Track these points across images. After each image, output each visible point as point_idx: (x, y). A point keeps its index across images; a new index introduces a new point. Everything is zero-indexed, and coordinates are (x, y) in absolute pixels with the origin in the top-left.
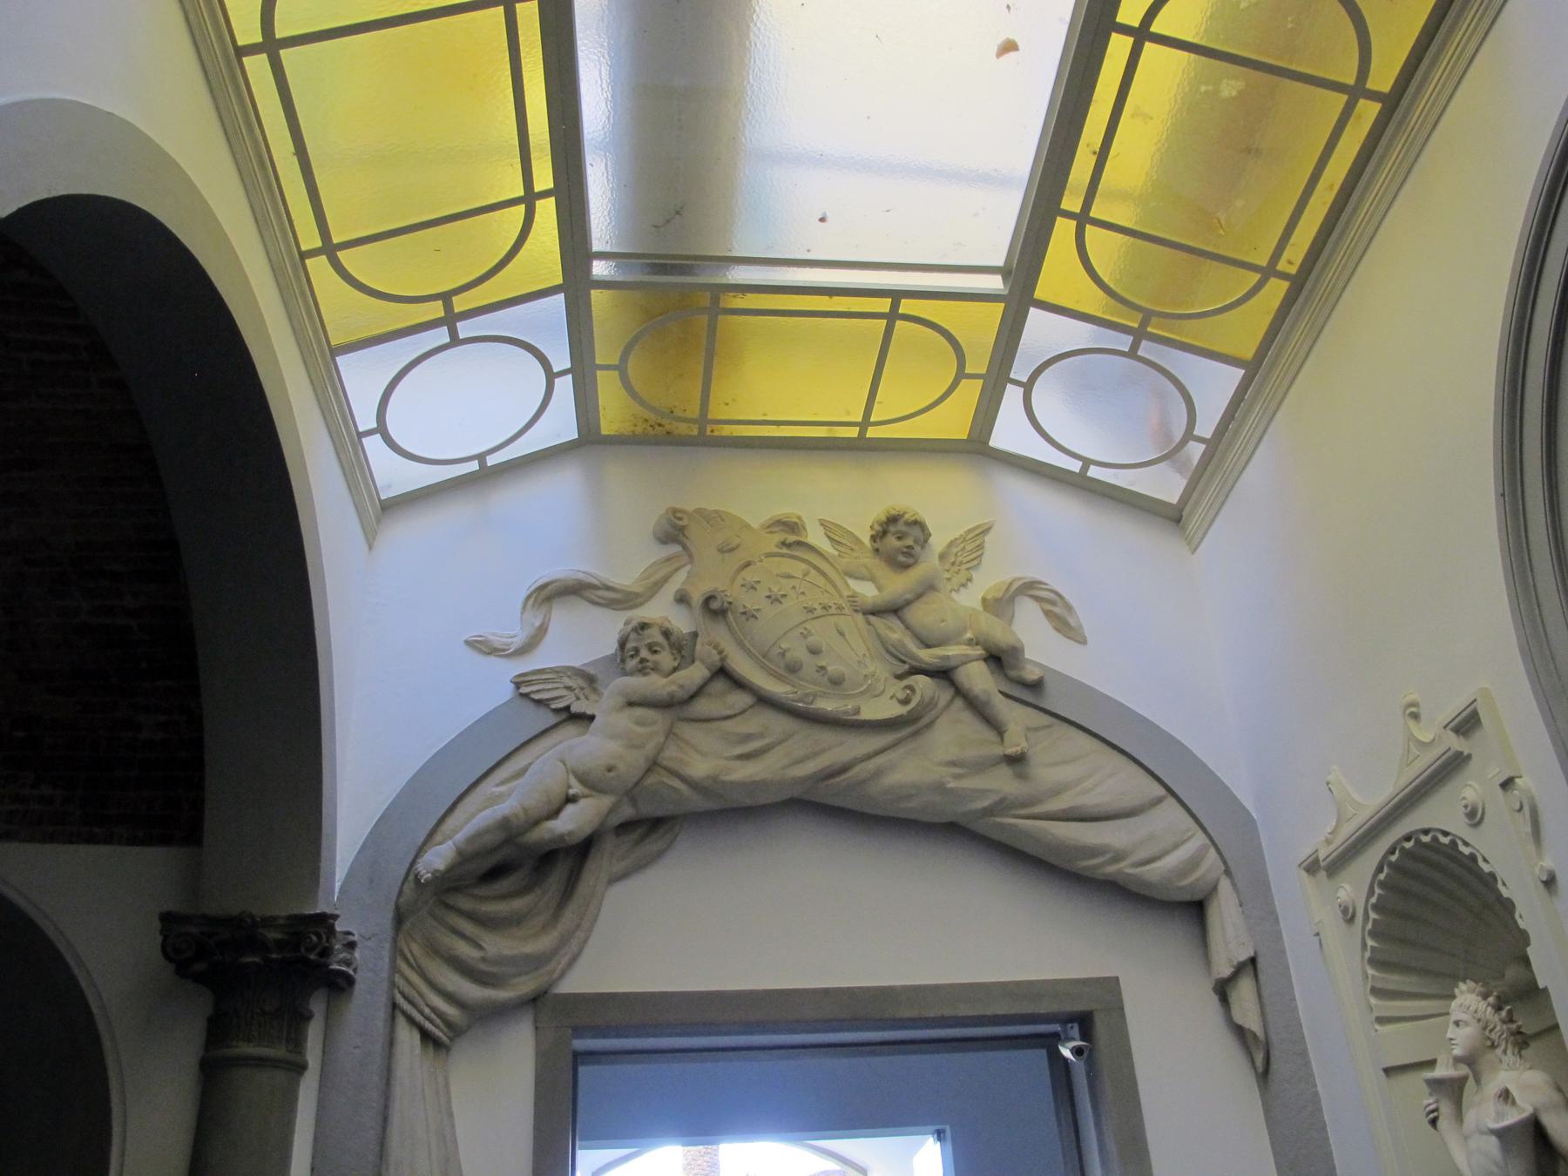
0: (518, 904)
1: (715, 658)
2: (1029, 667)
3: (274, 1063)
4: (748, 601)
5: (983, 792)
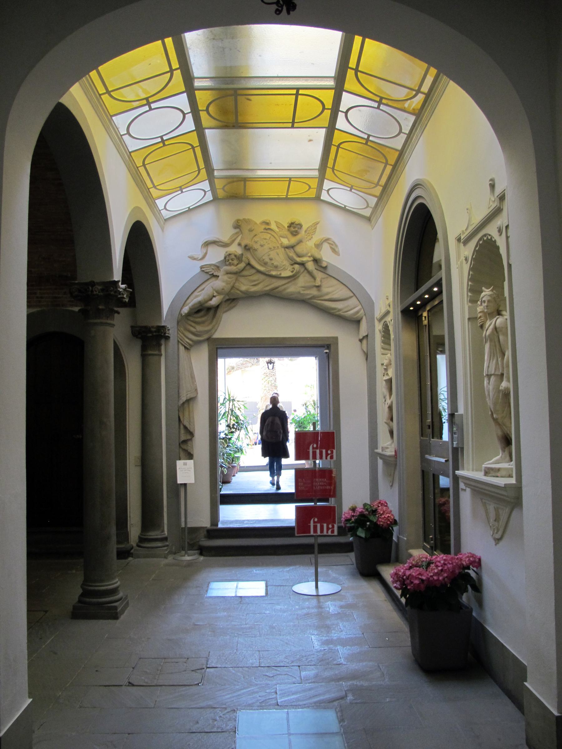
0: (203, 319)
1: (247, 261)
2: (324, 262)
3: (156, 355)
4: (256, 246)
5: (310, 294)
